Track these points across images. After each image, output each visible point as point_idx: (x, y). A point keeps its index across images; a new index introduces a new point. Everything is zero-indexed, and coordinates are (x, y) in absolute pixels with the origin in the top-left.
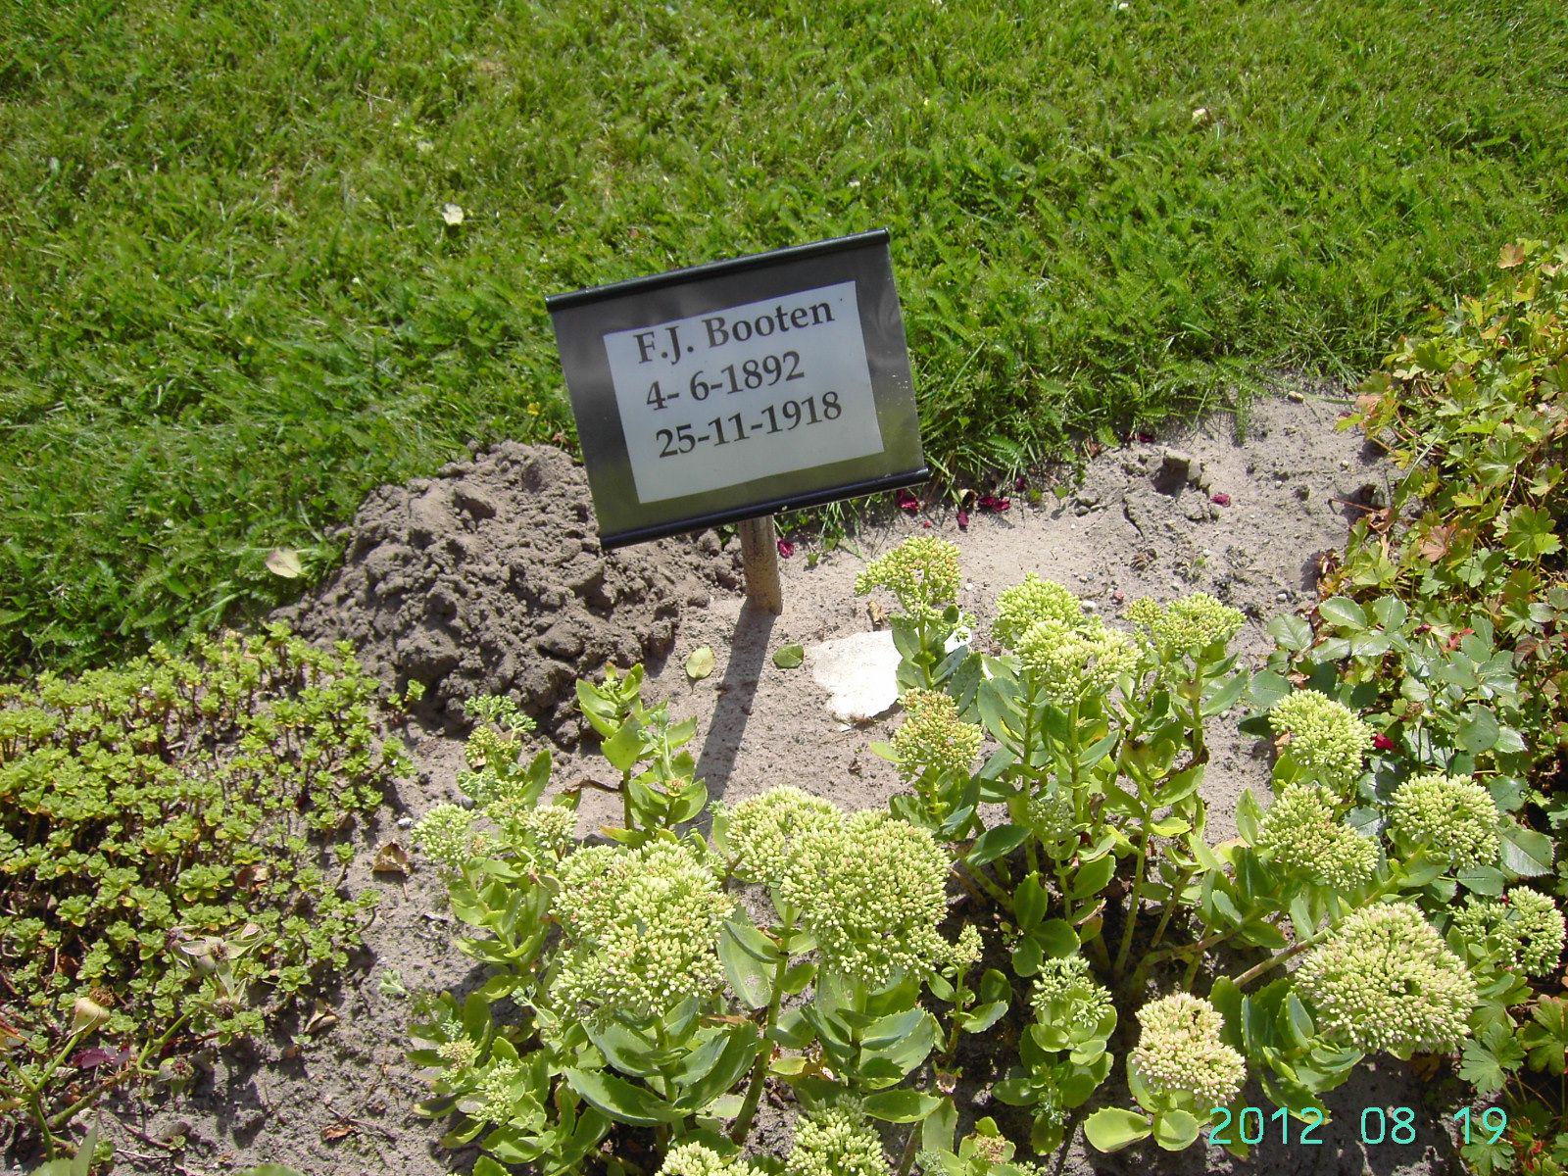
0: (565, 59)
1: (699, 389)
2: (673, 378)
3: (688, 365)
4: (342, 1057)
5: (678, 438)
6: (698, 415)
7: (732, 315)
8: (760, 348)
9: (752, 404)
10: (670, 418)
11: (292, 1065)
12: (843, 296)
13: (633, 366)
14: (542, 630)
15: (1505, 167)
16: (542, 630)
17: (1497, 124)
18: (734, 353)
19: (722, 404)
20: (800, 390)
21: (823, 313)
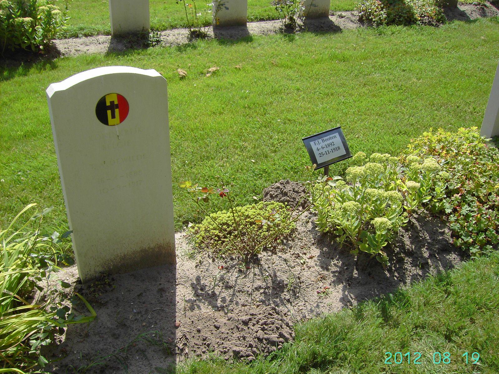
0: (258, 141)
1: (323, 148)
2: (319, 147)
3: (321, 145)
4: (299, 239)
5: (321, 155)
6: (323, 151)
7: (325, 138)
8: (329, 142)
9: (329, 149)
10: (320, 152)
11: (293, 240)
12: (337, 134)
13: (315, 145)
14: (300, 195)
15: (406, 136)
16: (300, 195)
17: (402, 130)
18: (326, 143)
19: (326, 149)
20: (335, 147)
21: (335, 137)
